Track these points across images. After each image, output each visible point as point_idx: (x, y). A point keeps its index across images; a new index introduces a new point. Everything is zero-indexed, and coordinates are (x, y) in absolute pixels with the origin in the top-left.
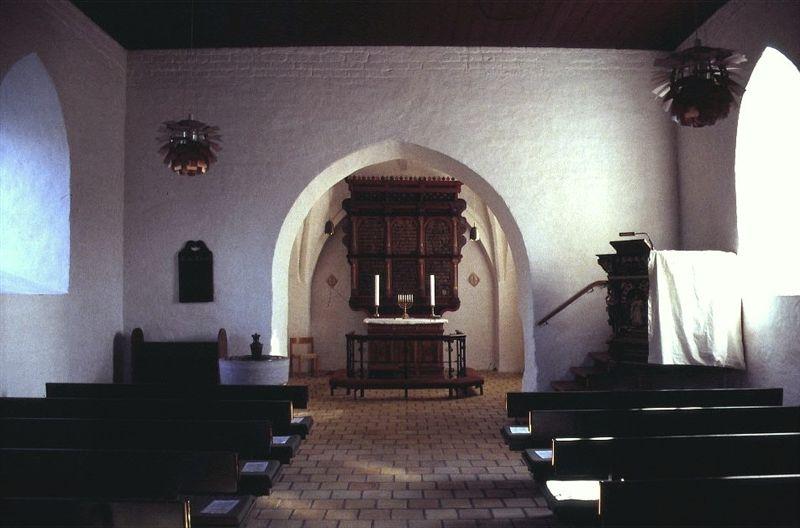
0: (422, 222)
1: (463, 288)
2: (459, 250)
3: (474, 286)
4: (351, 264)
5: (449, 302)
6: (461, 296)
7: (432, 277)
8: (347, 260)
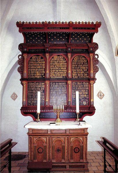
0: (48, 57)
1: (97, 102)
2: (94, 75)
3: (101, 98)
4: (23, 84)
5: (89, 110)
6: (95, 105)
7: (77, 93)
8: (20, 82)
